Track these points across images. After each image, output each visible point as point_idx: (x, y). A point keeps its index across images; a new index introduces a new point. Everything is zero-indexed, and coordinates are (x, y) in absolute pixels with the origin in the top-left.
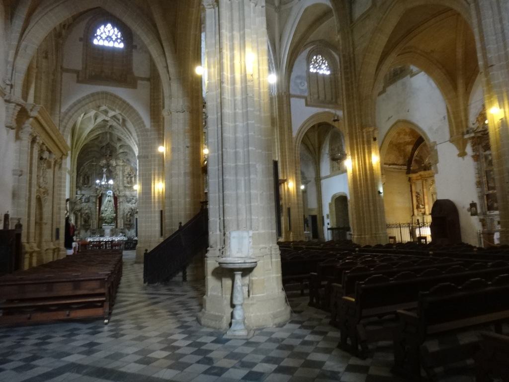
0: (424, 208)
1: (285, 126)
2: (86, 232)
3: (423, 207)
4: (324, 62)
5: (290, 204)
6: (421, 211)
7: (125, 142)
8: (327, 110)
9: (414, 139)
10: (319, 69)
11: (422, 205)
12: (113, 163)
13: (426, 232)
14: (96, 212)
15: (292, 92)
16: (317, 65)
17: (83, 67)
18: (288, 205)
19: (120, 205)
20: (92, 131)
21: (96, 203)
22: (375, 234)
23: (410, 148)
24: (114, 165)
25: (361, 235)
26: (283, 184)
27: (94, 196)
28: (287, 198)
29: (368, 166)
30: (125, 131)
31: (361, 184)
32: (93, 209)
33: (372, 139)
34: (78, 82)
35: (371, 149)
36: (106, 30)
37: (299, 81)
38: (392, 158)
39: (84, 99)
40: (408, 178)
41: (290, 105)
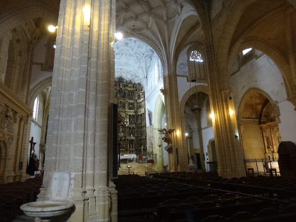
0: (273, 148)
1: (174, 94)
3: (272, 147)
4: (199, 54)
5: (177, 146)
6: (271, 150)
8: (202, 84)
9: (262, 101)
10: (195, 59)
11: (271, 146)
13: (275, 165)
15: (178, 73)
16: (194, 57)
17: (45, 62)
18: (177, 147)
22: (235, 168)
23: (259, 107)
25: (224, 169)
26: (172, 133)
28: (175, 142)
29: (226, 117)
31: (222, 131)
33: (228, 98)
34: (42, 70)
35: (228, 105)
37: (182, 66)
38: (248, 114)
39: (45, 80)
40: (260, 127)
41: (177, 82)
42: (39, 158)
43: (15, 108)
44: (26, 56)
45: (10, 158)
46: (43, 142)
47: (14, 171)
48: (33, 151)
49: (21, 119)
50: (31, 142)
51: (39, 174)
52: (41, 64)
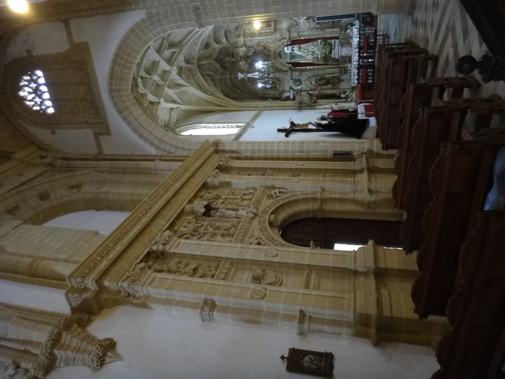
2: (342, 81)
7: (209, 36)
12: (242, 51)
14: (314, 70)
19: (304, 36)
20: (200, 88)
21: (301, 71)
24: (246, 50)
27: (292, 73)
30: (188, 41)
32: (310, 74)
34: (108, 132)
36: (30, 97)
39: (129, 124)
42: (328, 108)
43: (189, 192)
44: (80, 173)
45: (319, 190)
46: (293, 104)
47: (354, 172)
48: (310, 127)
49: (223, 169)
50: (287, 132)
51: (365, 106)
52: (97, 135)
